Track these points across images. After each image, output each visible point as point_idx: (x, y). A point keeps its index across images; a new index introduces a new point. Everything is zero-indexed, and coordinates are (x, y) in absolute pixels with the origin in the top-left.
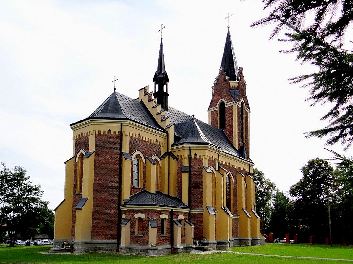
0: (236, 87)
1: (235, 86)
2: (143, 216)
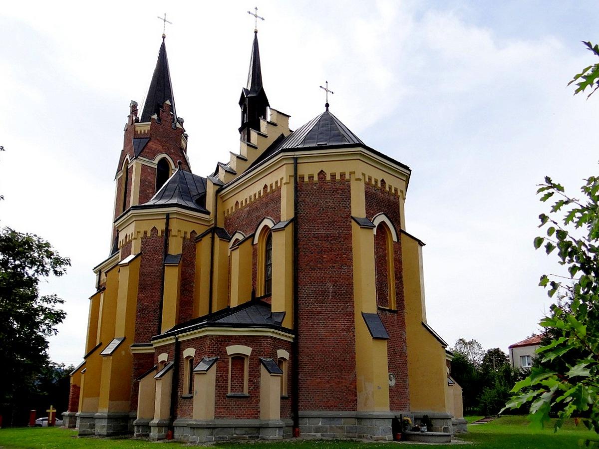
0: (146, 132)
2: (246, 350)
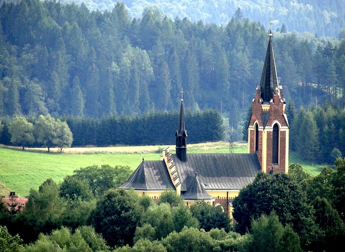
0: (268, 110)
1: (267, 110)
